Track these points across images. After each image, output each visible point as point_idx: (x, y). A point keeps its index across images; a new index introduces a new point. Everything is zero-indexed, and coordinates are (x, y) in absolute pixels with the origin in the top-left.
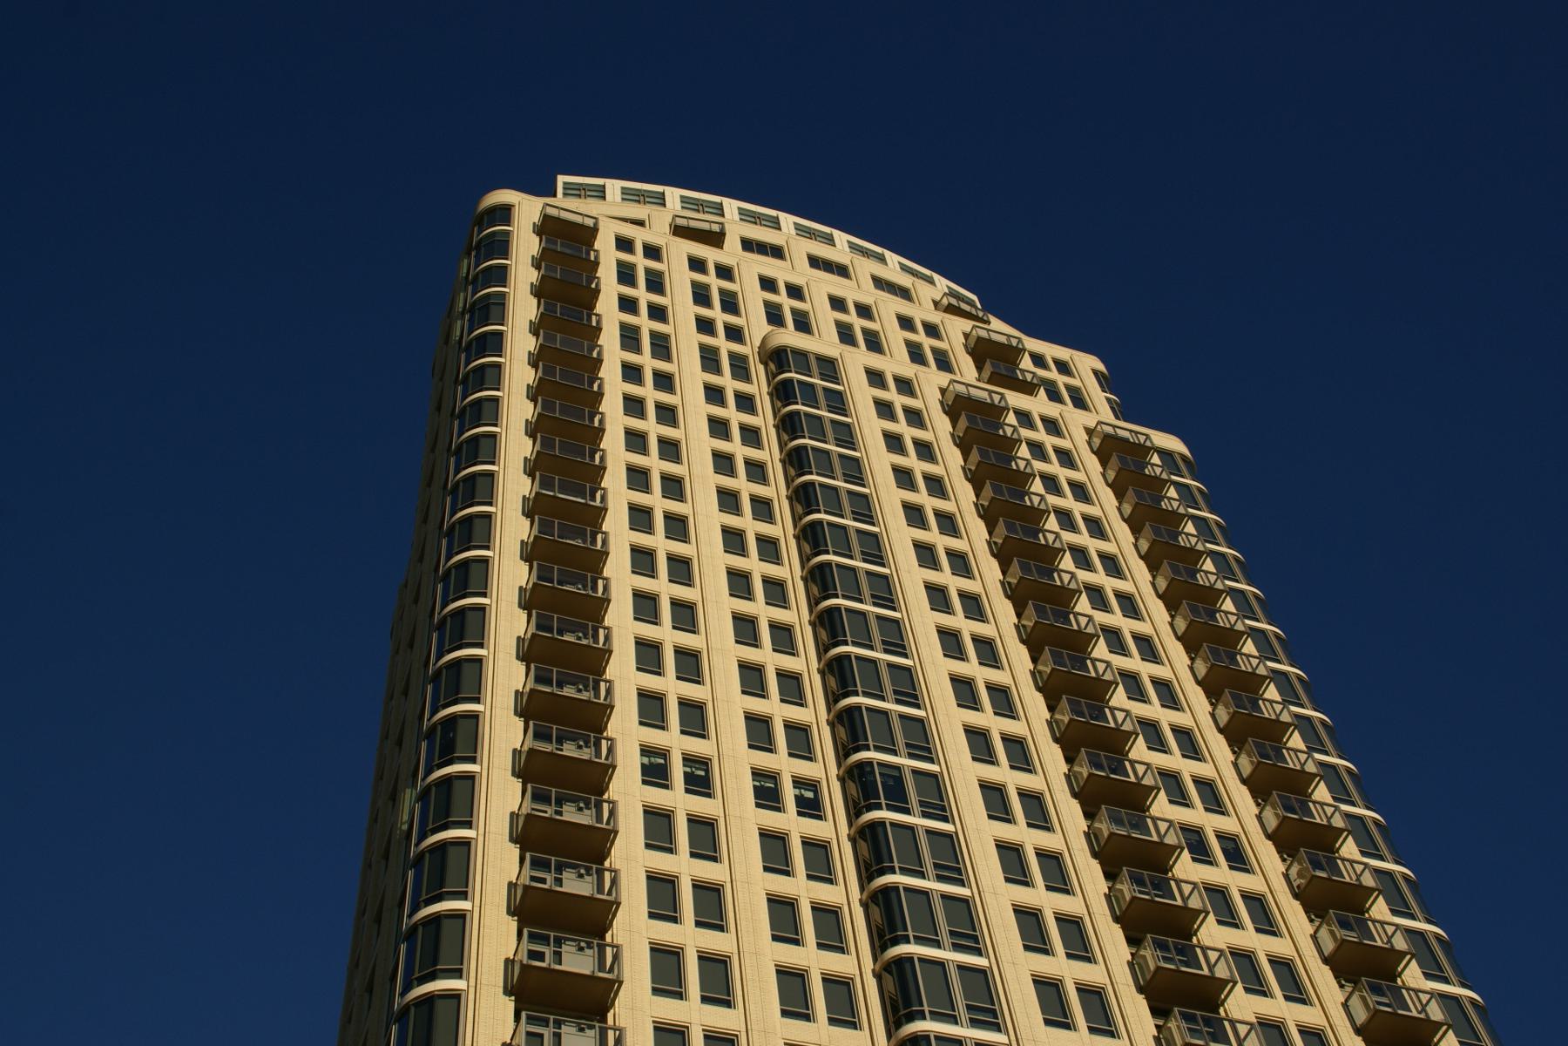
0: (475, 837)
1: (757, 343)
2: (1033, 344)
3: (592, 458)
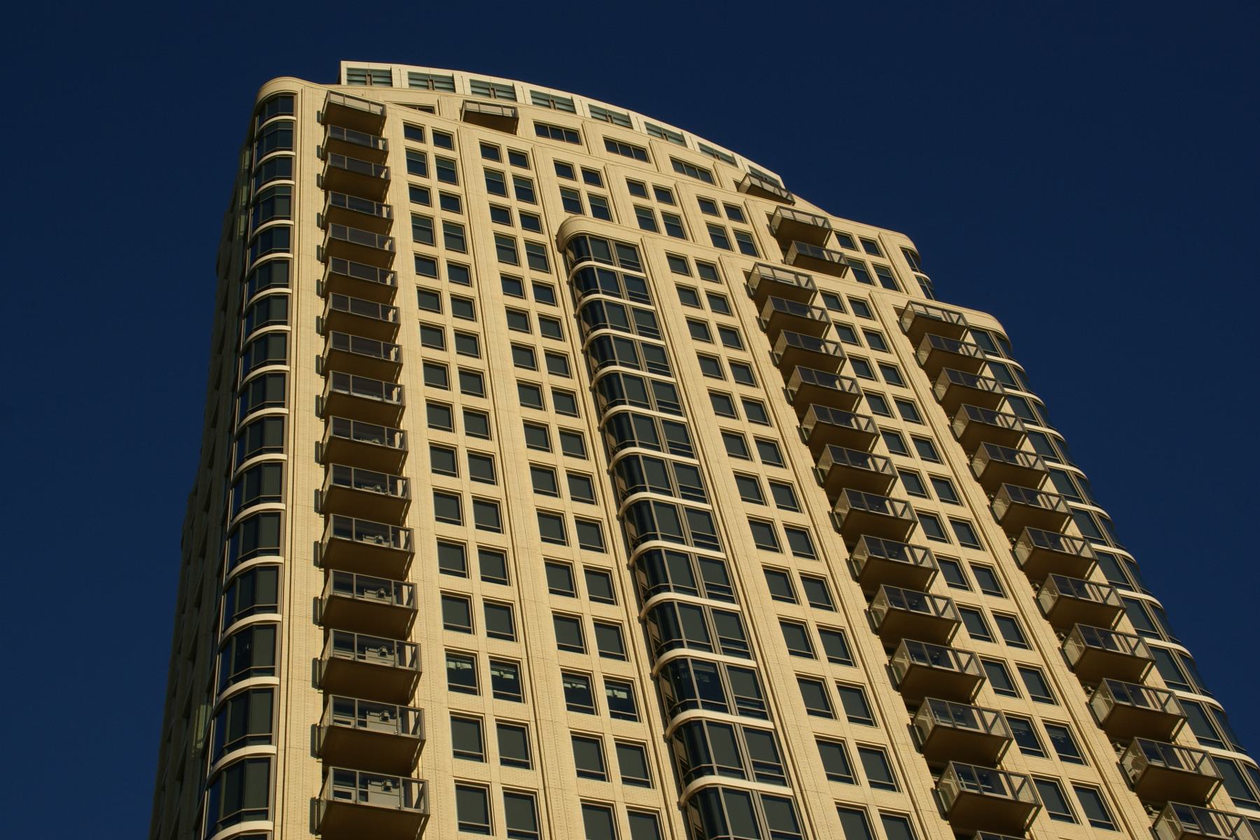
0: (278, 683)
1: (555, 231)
2: (840, 224)
3: (388, 354)
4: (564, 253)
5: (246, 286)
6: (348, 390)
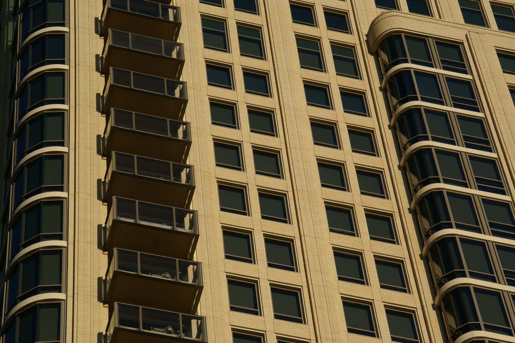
0: (66, 246)
1: (365, 30)
3: (178, 176)
4: (376, 55)
5: (17, 103)
6: (134, 218)
